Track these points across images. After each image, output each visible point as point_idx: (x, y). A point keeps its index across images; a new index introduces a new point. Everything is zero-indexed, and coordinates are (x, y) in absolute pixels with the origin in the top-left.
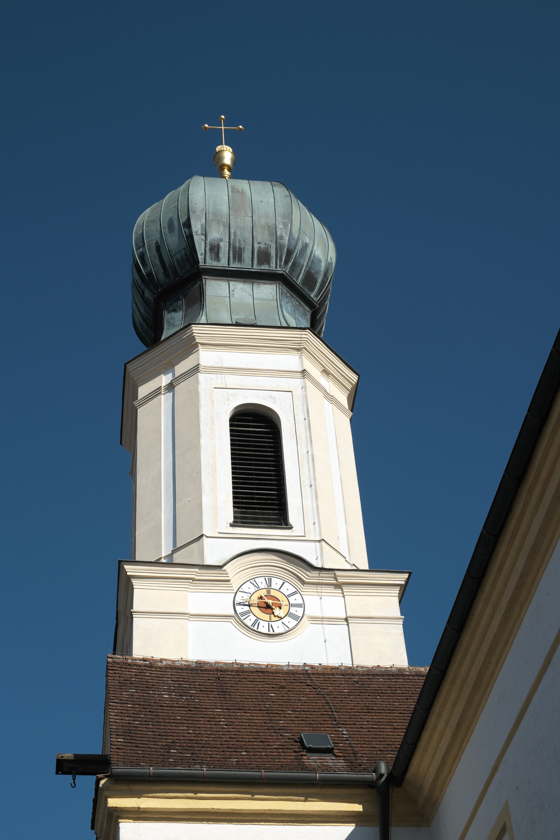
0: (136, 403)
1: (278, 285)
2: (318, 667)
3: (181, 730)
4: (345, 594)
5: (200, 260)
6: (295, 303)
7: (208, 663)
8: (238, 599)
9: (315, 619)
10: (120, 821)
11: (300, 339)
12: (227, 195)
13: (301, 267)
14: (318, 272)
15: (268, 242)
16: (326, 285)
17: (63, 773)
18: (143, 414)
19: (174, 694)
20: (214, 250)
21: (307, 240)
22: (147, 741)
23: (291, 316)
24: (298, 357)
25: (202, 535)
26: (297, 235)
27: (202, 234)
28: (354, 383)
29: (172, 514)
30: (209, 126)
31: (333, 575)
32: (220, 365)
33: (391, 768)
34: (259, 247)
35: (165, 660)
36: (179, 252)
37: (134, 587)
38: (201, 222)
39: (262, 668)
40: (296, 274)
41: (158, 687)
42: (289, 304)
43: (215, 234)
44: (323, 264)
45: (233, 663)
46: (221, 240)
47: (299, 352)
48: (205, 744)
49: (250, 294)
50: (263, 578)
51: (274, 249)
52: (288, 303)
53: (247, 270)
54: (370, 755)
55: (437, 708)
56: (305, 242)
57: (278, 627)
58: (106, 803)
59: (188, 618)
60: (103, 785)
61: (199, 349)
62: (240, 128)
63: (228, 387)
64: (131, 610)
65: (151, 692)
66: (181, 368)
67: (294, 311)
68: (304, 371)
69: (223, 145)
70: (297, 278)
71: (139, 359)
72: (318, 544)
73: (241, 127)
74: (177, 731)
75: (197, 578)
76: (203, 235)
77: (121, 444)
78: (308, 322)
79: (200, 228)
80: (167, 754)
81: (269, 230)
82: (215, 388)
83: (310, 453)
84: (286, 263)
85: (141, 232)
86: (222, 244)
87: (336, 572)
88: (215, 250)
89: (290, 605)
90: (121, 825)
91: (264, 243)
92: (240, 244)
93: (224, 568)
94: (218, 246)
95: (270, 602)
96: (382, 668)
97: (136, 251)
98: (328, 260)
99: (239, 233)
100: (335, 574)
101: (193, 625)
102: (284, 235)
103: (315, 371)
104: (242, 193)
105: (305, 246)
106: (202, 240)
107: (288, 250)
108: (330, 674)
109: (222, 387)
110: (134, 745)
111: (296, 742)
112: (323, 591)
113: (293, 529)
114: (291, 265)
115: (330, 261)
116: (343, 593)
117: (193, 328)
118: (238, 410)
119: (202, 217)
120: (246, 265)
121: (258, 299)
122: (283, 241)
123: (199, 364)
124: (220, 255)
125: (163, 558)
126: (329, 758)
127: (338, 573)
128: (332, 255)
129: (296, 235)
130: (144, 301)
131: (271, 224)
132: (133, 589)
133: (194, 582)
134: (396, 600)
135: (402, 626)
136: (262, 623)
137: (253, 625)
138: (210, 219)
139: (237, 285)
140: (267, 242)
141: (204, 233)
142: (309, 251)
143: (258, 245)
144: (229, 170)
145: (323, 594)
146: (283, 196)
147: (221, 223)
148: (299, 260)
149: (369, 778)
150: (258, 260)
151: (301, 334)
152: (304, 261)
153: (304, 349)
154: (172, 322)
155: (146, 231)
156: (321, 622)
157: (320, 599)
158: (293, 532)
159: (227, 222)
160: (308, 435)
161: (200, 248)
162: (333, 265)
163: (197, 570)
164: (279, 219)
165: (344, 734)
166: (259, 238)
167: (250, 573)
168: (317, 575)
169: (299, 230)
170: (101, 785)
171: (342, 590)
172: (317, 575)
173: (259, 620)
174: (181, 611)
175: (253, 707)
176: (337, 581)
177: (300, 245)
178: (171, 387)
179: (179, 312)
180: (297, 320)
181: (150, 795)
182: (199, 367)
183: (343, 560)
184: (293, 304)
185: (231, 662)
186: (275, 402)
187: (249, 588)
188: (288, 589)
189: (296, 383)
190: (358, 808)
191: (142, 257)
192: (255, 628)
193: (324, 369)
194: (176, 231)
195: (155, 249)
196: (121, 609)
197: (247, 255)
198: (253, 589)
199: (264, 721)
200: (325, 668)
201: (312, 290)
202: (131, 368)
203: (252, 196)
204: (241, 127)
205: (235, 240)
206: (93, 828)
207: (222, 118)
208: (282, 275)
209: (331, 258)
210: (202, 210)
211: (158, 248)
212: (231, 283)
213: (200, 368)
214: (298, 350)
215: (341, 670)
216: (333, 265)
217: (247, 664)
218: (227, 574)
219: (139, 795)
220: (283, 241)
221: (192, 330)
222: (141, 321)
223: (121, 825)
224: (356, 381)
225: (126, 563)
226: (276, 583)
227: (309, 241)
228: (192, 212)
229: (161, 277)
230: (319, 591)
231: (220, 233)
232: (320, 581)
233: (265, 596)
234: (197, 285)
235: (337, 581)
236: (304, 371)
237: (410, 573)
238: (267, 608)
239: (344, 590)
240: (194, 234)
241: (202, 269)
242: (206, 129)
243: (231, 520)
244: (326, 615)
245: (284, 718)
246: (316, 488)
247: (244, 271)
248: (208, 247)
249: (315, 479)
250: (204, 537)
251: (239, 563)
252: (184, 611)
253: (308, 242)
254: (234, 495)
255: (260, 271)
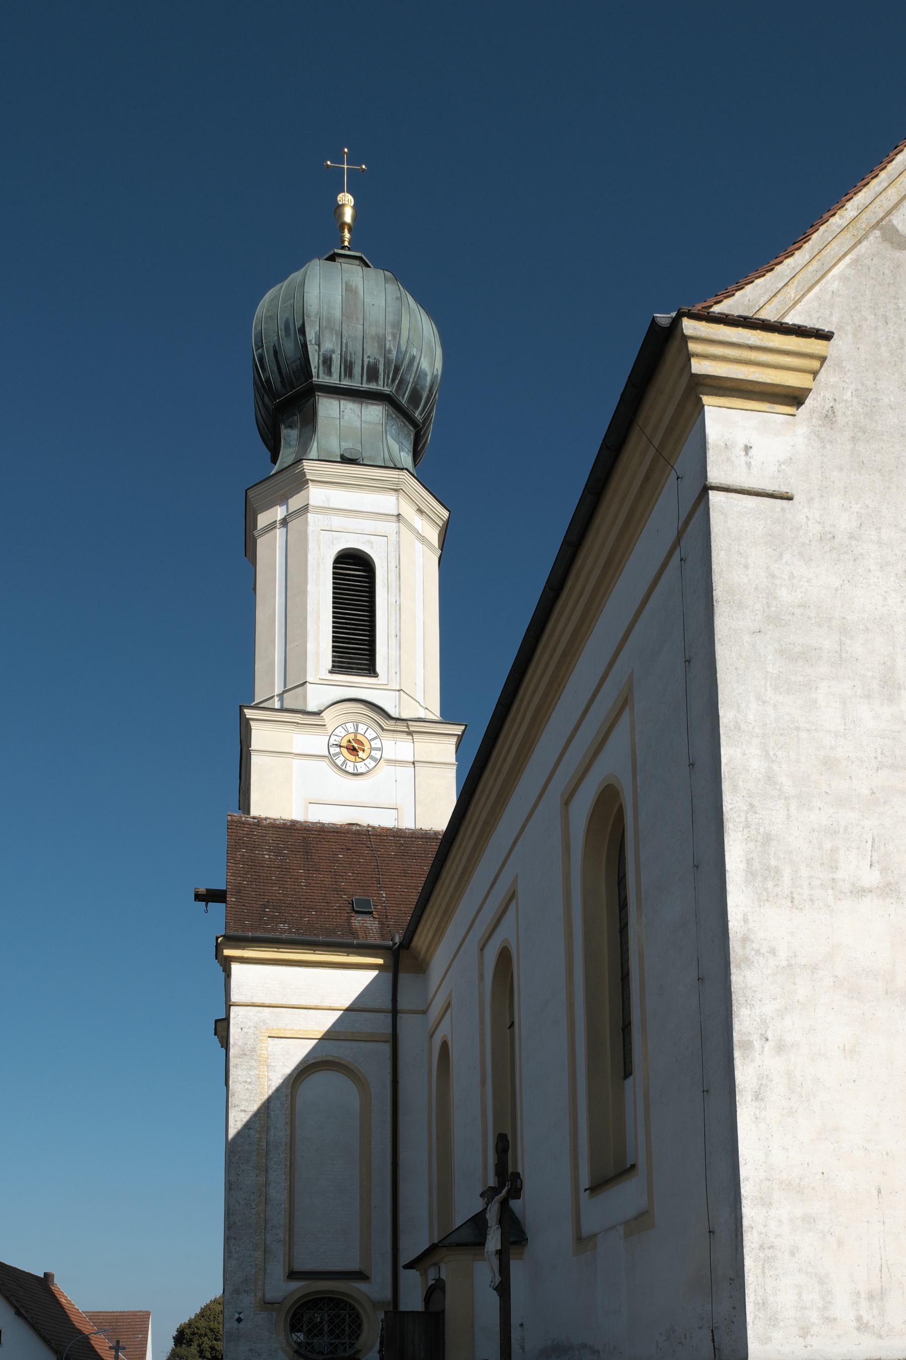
0: (256, 533)
1: (384, 406)
2: (378, 828)
3: (274, 890)
4: (415, 740)
5: (313, 373)
6: (400, 424)
7: (299, 822)
8: (332, 742)
9: (389, 761)
10: (232, 963)
11: (397, 480)
12: (341, 294)
13: (407, 383)
14: (423, 388)
15: (378, 357)
16: (430, 403)
17: (199, 901)
18: (262, 544)
19: (272, 854)
20: (327, 362)
21: (414, 352)
22: (251, 900)
23: (395, 441)
24: (395, 498)
25: (306, 682)
26: (405, 348)
27: (316, 344)
28: (445, 520)
29: (284, 654)
30: (331, 163)
31: (406, 725)
32: (326, 506)
33: (402, 938)
34: (369, 362)
35: (269, 819)
36: (294, 362)
37: (252, 727)
38: (315, 329)
39: (337, 828)
40: (401, 392)
41: (262, 846)
42: (394, 427)
43: (329, 344)
44: (429, 378)
45: (316, 823)
46: (333, 351)
47: (397, 493)
48: (289, 904)
49: (359, 416)
50: (352, 723)
51: (383, 365)
52: (393, 426)
53: (356, 388)
54: (397, 918)
55: (425, 916)
56: (412, 354)
57: (361, 768)
58: (223, 953)
59: (292, 756)
60: (221, 941)
61: (308, 487)
62: (362, 168)
63: (333, 530)
64: (250, 749)
65: (257, 852)
66: (295, 502)
67: (399, 434)
68: (399, 515)
69: (344, 192)
70: (403, 396)
71: (257, 486)
72: (397, 693)
73: (364, 167)
74: (271, 891)
75: (300, 722)
76: (317, 345)
77: (246, 556)
78: (411, 444)
79: (314, 337)
80: (263, 913)
81: (378, 341)
82: (322, 530)
83: (398, 602)
84: (393, 381)
85: (260, 328)
86: (334, 356)
87: (408, 722)
88: (327, 362)
89: (371, 749)
90: (232, 966)
91: (373, 358)
92: (351, 357)
93: (322, 715)
94: (331, 358)
95: (356, 745)
96: (423, 830)
97: (256, 351)
98: (434, 372)
99: (350, 344)
100: (407, 724)
101: (296, 763)
102: (393, 349)
103: (408, 511)
104: (355, 292)
105: (413, 358)
106: (316, 350)
107: (395, 366)
108: (385, 836)
109: (327, 529)
110: (242, 904)
111: (349, 904)
112: (397, 737)
113: (379, 677)
114: (398, 383)
115: (436, 373)
116: (413, 740)
117: (304, 464)
118: (340, 553)
119: (316, 323)
120: (355, 383)
121: (365, 422)
122: (391, 356)
123: (308, 504)
124: (332, 368)
125: (276, 697)
126: (369, 919)
127: (410, 723)
128: (439, 365)
129: (403, 349)
130: (264, 405)
131: (381, 334)
132: (251, 729)
133: (298, 725)
134: (453, 748)
135: (455, 770)
136: (349, 763)
137: (342, 765)
138: (324, 325)
139: (348, 404)
140: (376, 356)
141: (317, 343)
142: (415, 364)
143: (368, 360)
144: (350, 231)
145: (397, 739)
146: (394, 298)
147: (334, 332)
148: (405, 376)
149: (387, 945)
150: (367, 376)
151: (399, 475)
152: (410, 377)
153: (401, 490)
154: (288, 439)
155: (264, 329)
156: (394, 764)
157: (395, 743)
158: (378, 680)
159: (339, 330)
160: (398, 584)
161: (314, 360)
162: (439, 377)
163: (300, 715)
164: (389, 330)
165: (383, 897)
166: (369, 352)
167: (343, 719)
168: (394, 724)
169: (408, 341)
170: (219, 942)
171: (413, 737)
172: (394, 724)
173: (347, 761)
174: (287, 751)
175: (326, 868)
176: (409, 729)
177: (407, 359)
178: (285, 522)
179: (294, 429)
180: (400, 443)
181: (250, 949)
182: (307, 508)
183: (418, 704)
184: (398, 425)
185: (316, 821)
186: (372, 547)
187: (340, 732)
188: (371, 734)
189: (391, 527)
190: (380, 961)
191: (261, 358)
192: (344, 767)
193: (418, 508)
194: (292, 336)
195: (273, 353)
196: (243, 738)
197: (357, 370)
198: (343, 733)
199: (331, 883)
200: (383, 829)
201: (417, 408)
202: (252, 494)
203: (365, 297)
204: (364, 167)
205: (346, 352)
206: (216, 959)
207: (345, 152)
208: (389, 395)
209: (437, 370)
210: (317, 315)
211: (276, 353)
212: (342, 402)
213: (309, 508)
214: (396, 490)
215: (394, 832)
216: (439, 377)
217: (327, 824)
218: (324, 720)
219: (243, 948)
220: (391, 356)
221: (303, 466)
222: (263, 424)
223: (232, 966)
224: (447, 518)
225: (245, 707)
226: (362, 728)
227: (416, 352)
228: (307, 317)
229: (279, 385)
230: (394, 736)
231: (333, 344)
232: (396, 729)
233: (353, 739)
234: (310, 401)
235: (409, 729)
236: (399, 515)
237: (466, 726)
238: (353, 750)
239: (414, 737)
240: (308, 343)
241: (315, 384)
242: (328, 168)
243: (330, 666)
244: (398, 758)
245: (345, 881)
246: (400, 639)
247: (354, 389)
248: (321, 359)
249: (400, 629)
250: (308, 683)
251: (333, 710)
252: (290, 751)
253: (415, 354)
254: (334, 639)
255: (368, 389)
